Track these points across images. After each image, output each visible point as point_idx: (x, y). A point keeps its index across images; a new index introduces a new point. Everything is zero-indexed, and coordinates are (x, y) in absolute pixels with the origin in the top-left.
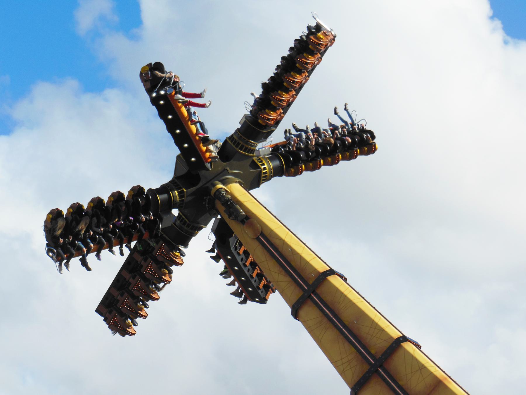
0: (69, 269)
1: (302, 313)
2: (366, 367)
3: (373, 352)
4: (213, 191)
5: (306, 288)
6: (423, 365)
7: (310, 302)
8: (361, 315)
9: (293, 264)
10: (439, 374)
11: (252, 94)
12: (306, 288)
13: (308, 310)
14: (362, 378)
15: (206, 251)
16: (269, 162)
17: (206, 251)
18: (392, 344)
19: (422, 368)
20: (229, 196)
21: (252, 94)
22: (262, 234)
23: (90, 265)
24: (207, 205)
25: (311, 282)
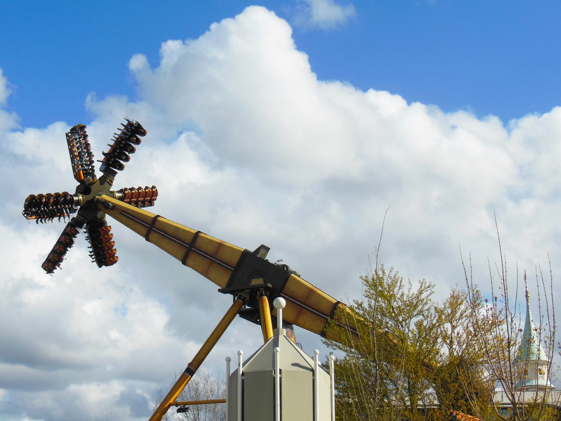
0: (53, 222)
1: (150, 237)
2: (186, 249)
3: (187, 242)
4: (96, 199)
5: (111, 168)
6: (211, 240)
7: (152, 232)
8: (177, 229)
9: (140, 218)
10: (219, 241)
11: (61, 269)
12: (111, 168)
13: (153, 236)
14: (185, 255)
15: (108, 144)
16: (243, 381)
17: (108, 144)
18: (195, 236)
19: (211, 241)
20: (103, 200)
21: (61, 269)
22: (122, 211)
23: (60, 220)
24: (94, 208)
25: (150, 223)
